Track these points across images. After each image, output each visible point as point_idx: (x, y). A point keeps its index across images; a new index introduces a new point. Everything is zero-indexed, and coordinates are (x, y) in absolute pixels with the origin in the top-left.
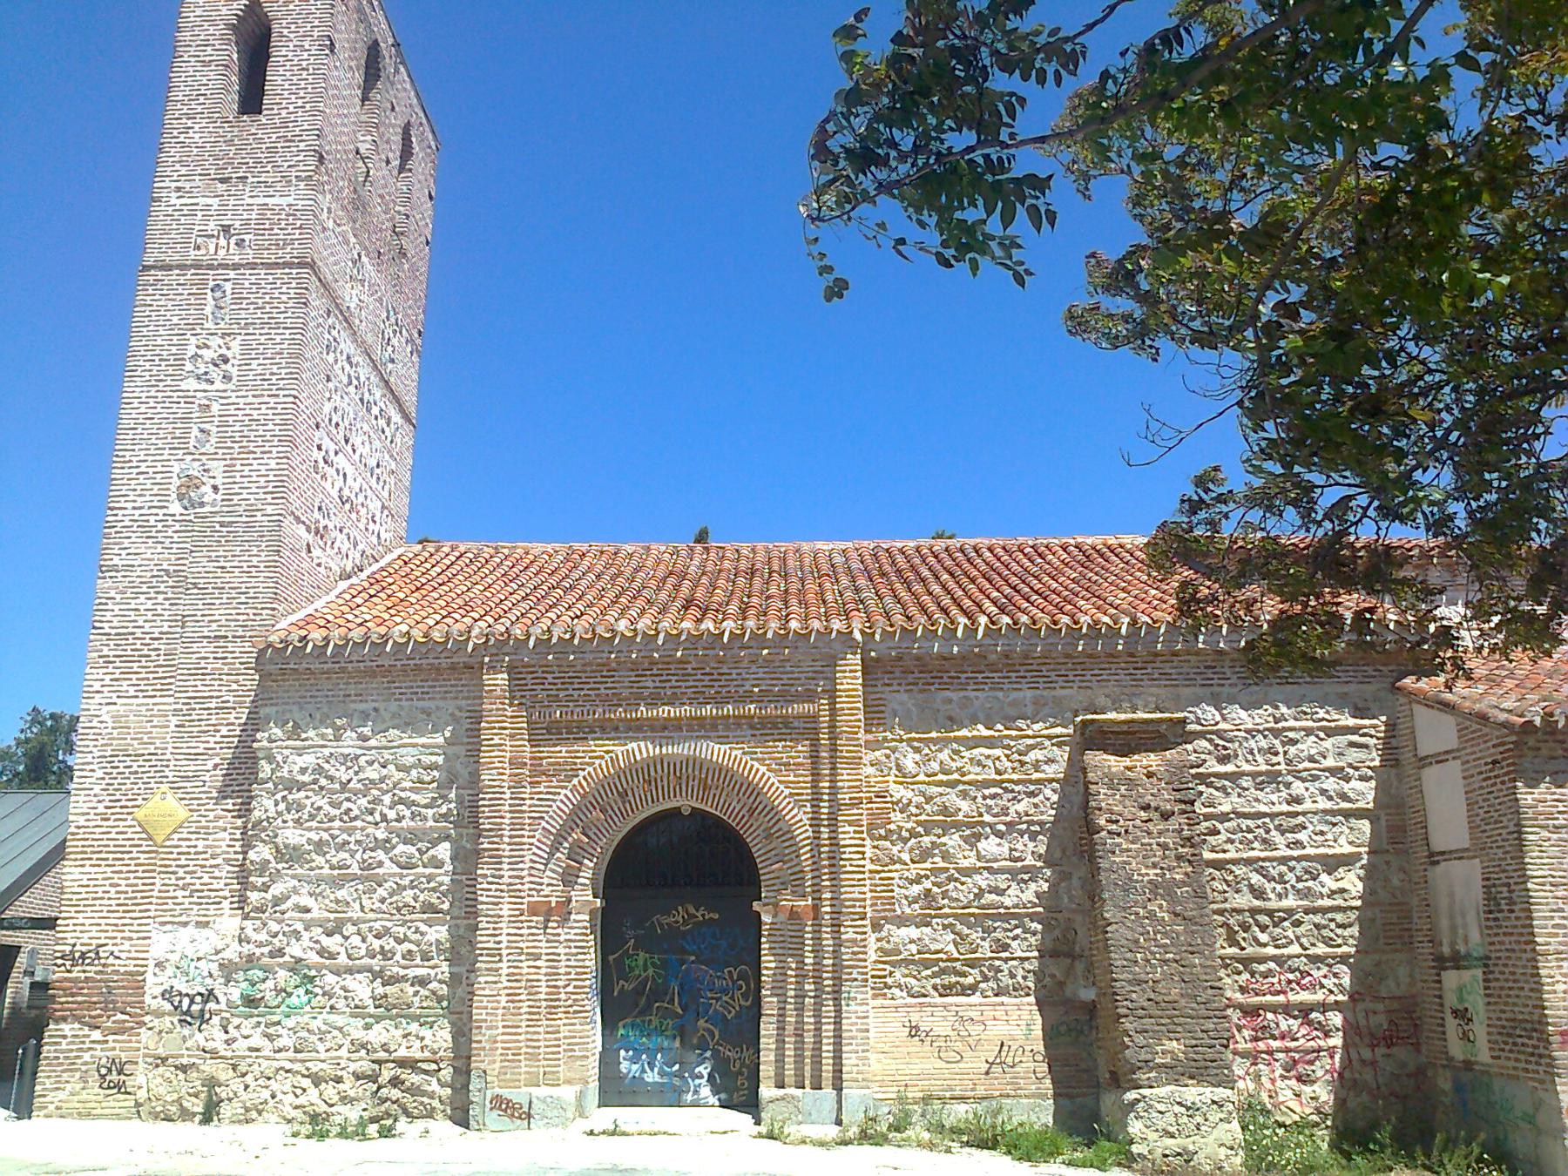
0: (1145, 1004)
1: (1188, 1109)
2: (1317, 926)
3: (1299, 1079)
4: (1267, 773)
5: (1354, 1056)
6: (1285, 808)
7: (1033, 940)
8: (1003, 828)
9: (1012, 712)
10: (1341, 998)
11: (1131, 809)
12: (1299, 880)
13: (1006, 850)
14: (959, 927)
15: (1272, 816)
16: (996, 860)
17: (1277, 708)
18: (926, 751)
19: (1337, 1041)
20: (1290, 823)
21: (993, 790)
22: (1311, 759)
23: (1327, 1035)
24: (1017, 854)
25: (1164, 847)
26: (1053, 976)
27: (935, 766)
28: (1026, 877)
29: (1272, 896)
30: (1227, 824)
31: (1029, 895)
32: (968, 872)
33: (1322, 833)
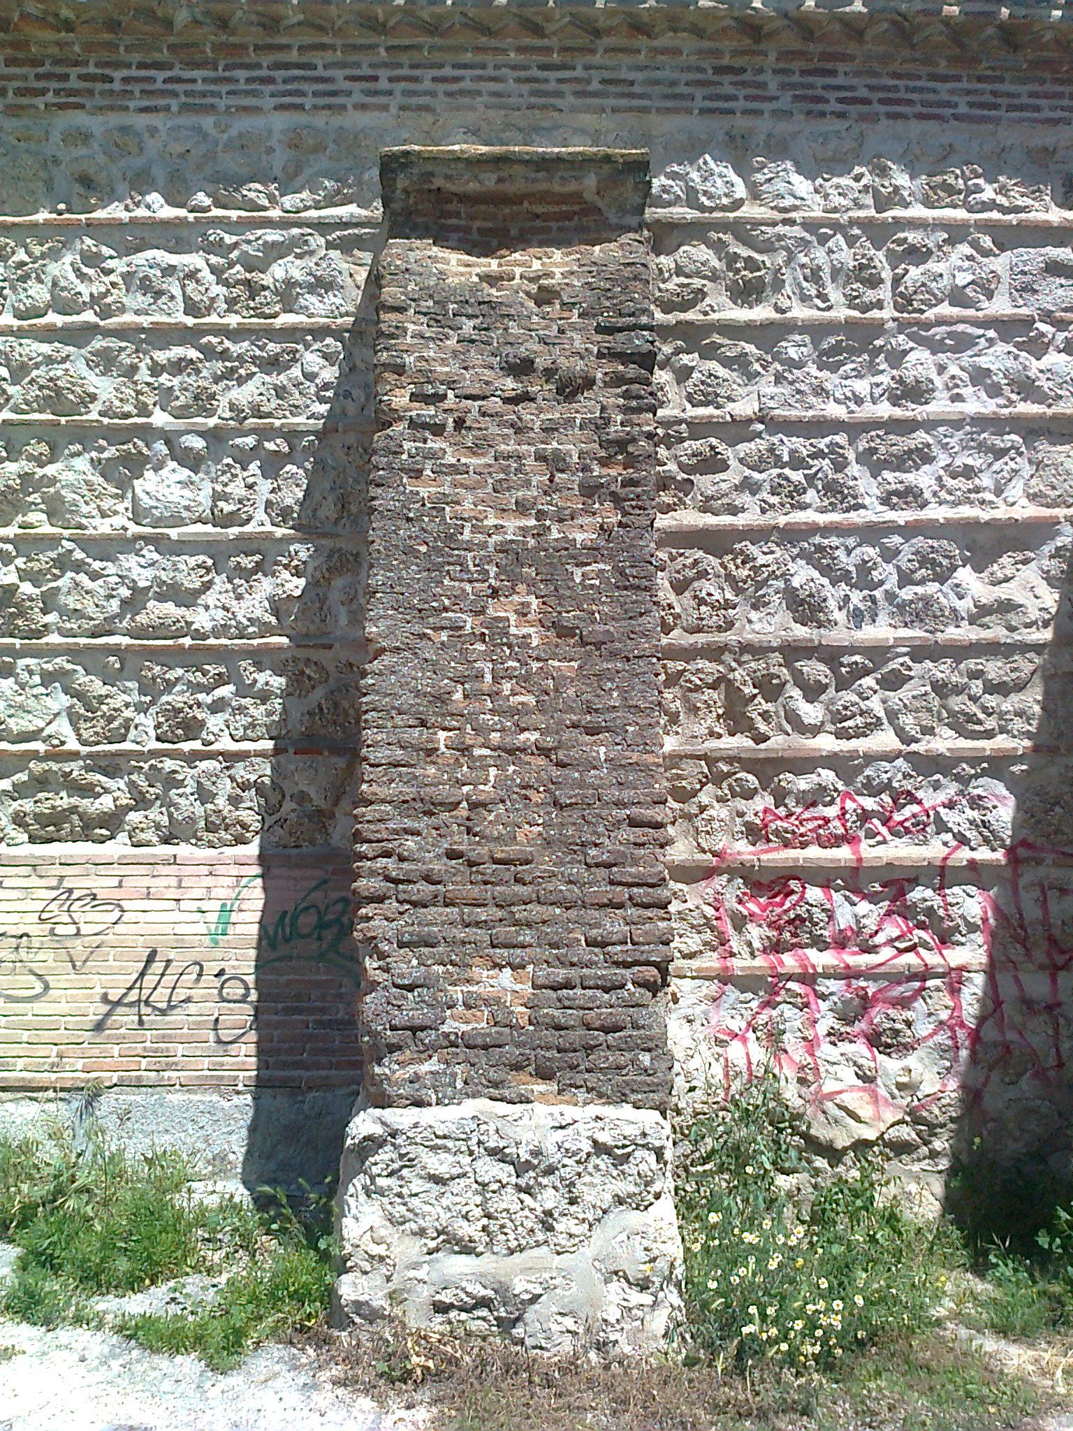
0: (437, 867)
1: (521, 1168)
2: (941, 688)
3: (875, 1040)
4: (849, 324)
5: (1008, 990)
6: (884, 410)
7: (258, 712)
8: (198, 443)
9: (230, 162)
10: (983, 854)
11: (481, 371)
12: (906, 579)
13: (204, 497)
14: (82, 678)
15: (855, 429)
16: (178, 521)
17: (883, 172)
18: (21, 255)
19: (970, 954)
20: (893, 446)
21: (176, 352)
22: (957, 297)
23: (945, 939)
24: (228, 508)
25: (555, 463)
26: (302, 797)
27: (39, 293)
28: (248, 562)
29: (839, 616)
30: (743, 448)
31: (255, 603)
32: (109, 548)
33: (968, 472)
